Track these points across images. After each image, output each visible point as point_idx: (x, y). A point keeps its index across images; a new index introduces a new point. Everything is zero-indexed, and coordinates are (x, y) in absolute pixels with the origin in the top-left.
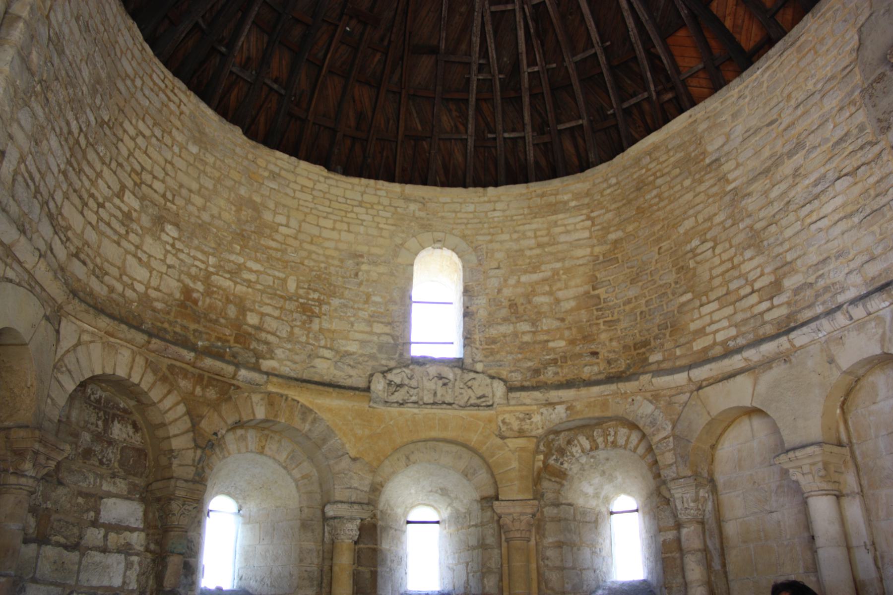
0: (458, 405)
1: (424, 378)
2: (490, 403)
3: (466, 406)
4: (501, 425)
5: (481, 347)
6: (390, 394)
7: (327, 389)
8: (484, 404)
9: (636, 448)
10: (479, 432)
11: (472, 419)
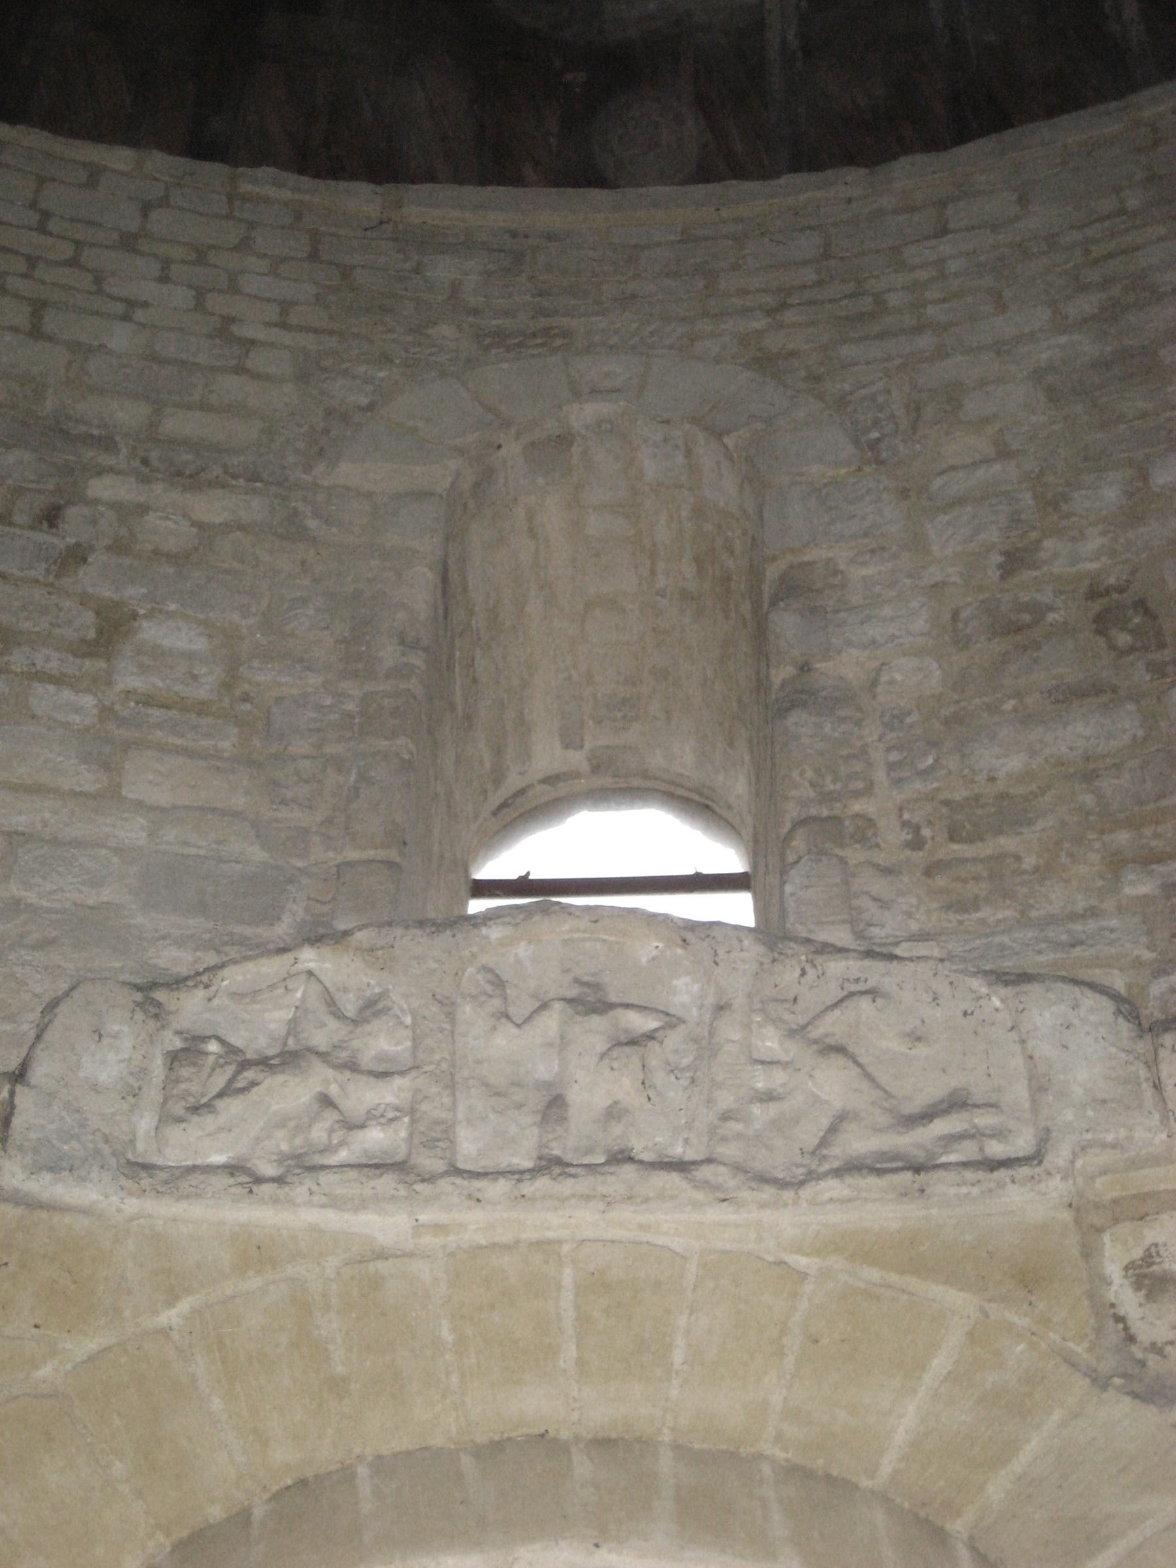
0: (738, 1168)
1: (467, 1010)
2: (1022, 1144)
3: (812, 1176)
4: (1129, 1301)
5: (918, 856)
6: (178, 1109)
7: (345, 1169)
8: (967, 1151)
9: (1159, 1263)
10: (940, 1363)
11: (873, 1274)
